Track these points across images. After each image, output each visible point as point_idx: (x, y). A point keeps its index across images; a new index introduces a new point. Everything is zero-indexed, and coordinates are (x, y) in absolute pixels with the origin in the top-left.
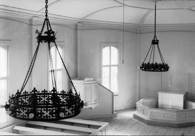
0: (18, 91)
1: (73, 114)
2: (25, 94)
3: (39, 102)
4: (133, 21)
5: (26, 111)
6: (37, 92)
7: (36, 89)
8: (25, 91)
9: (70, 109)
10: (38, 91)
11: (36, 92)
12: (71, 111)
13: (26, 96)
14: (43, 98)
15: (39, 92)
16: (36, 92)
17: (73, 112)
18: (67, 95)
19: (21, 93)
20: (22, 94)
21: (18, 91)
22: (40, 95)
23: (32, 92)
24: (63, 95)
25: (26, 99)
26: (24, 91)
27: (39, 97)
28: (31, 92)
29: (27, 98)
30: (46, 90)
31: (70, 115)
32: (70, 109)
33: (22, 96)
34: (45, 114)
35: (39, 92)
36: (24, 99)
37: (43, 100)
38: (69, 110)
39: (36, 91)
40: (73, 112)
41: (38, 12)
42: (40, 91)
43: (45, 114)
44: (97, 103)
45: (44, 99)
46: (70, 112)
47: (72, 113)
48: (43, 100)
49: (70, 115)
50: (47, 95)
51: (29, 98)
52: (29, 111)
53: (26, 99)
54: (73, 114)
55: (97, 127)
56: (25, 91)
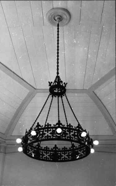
1: (85, 155)
3: (41, 157)
4: (58, 89)
5: (49, 154)
6: (41, 127)
9: (82, 151)
10: (41, 126)
11: (40, 127)
12: (83, 152)
13: (49, 128)
15: (42, 126)
16: (40, 127)
17: (85, 153)
22: (43, 130)
23: (56, 125)
24: (47, 150)
25: (49, 132)
28: (55, 124)
29: (50, 130)
30: (66, 147)
32: (82, 151)
35: (42, 126)
36: (47, 132)
38: (81, 152)
39: (40, 126)
40: (85, 153)
41: (35, 89)
46: (82, 154)
47: (84, 154)
48: (63, 157)
49: (80, 150)
50: (51, 128)
51: (52, 131)
52: (52, 154)
53: (49, 132)
54: (85, 155)
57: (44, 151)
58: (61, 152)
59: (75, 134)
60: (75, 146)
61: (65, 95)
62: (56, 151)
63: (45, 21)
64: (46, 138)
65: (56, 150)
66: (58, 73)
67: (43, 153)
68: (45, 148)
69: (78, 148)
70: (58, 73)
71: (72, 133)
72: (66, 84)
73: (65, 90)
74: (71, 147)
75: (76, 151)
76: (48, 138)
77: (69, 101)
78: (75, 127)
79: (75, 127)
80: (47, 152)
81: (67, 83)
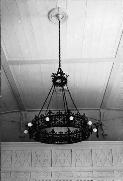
0: (36, 115)
2: (59, 114)
6: (72, 114)
7: (54, 73)
8: (42, 114)
12: (40, 124)
14: (77, 121)
18: (64, 115)
19: (38, 117)
20: (39, 117)
21: (36, 115)
26: (40, 115)
27: (54, 118)
31: (75, 134)
33: (39, 119)
34: (58, 120)
35: (57, 133)
37: (61, 119)
39: (54, 132)
42: (74, 113)
43: (58, 120)
44: (38, 116)
45: (59, 120)
46: (40, 122)
47: (38, 122)
48: (61, 119)
55: (2, 65)
56: (42, 114)
57: (56, 117)
58: (73, 135)
59: (82, 122)
60: (70, 131)
61: (66, 85)
62: (61, 135)
63: (51, 91)
64: (61, 117)
65: (69, 133)
66: (60, 66)
67: (56, 118)
68: (75, 131)
69: (73, 133)
70: (60, 66)
71: (79, 121)
72: (67, 76)
73: (66, 81)
74: (67, 132)
75: (72, 135)
76: (60, 125)
77: (70, 92)
78: (49, 132)
79: (49, 132)
80: (54, 121)
81: (68, 76)
